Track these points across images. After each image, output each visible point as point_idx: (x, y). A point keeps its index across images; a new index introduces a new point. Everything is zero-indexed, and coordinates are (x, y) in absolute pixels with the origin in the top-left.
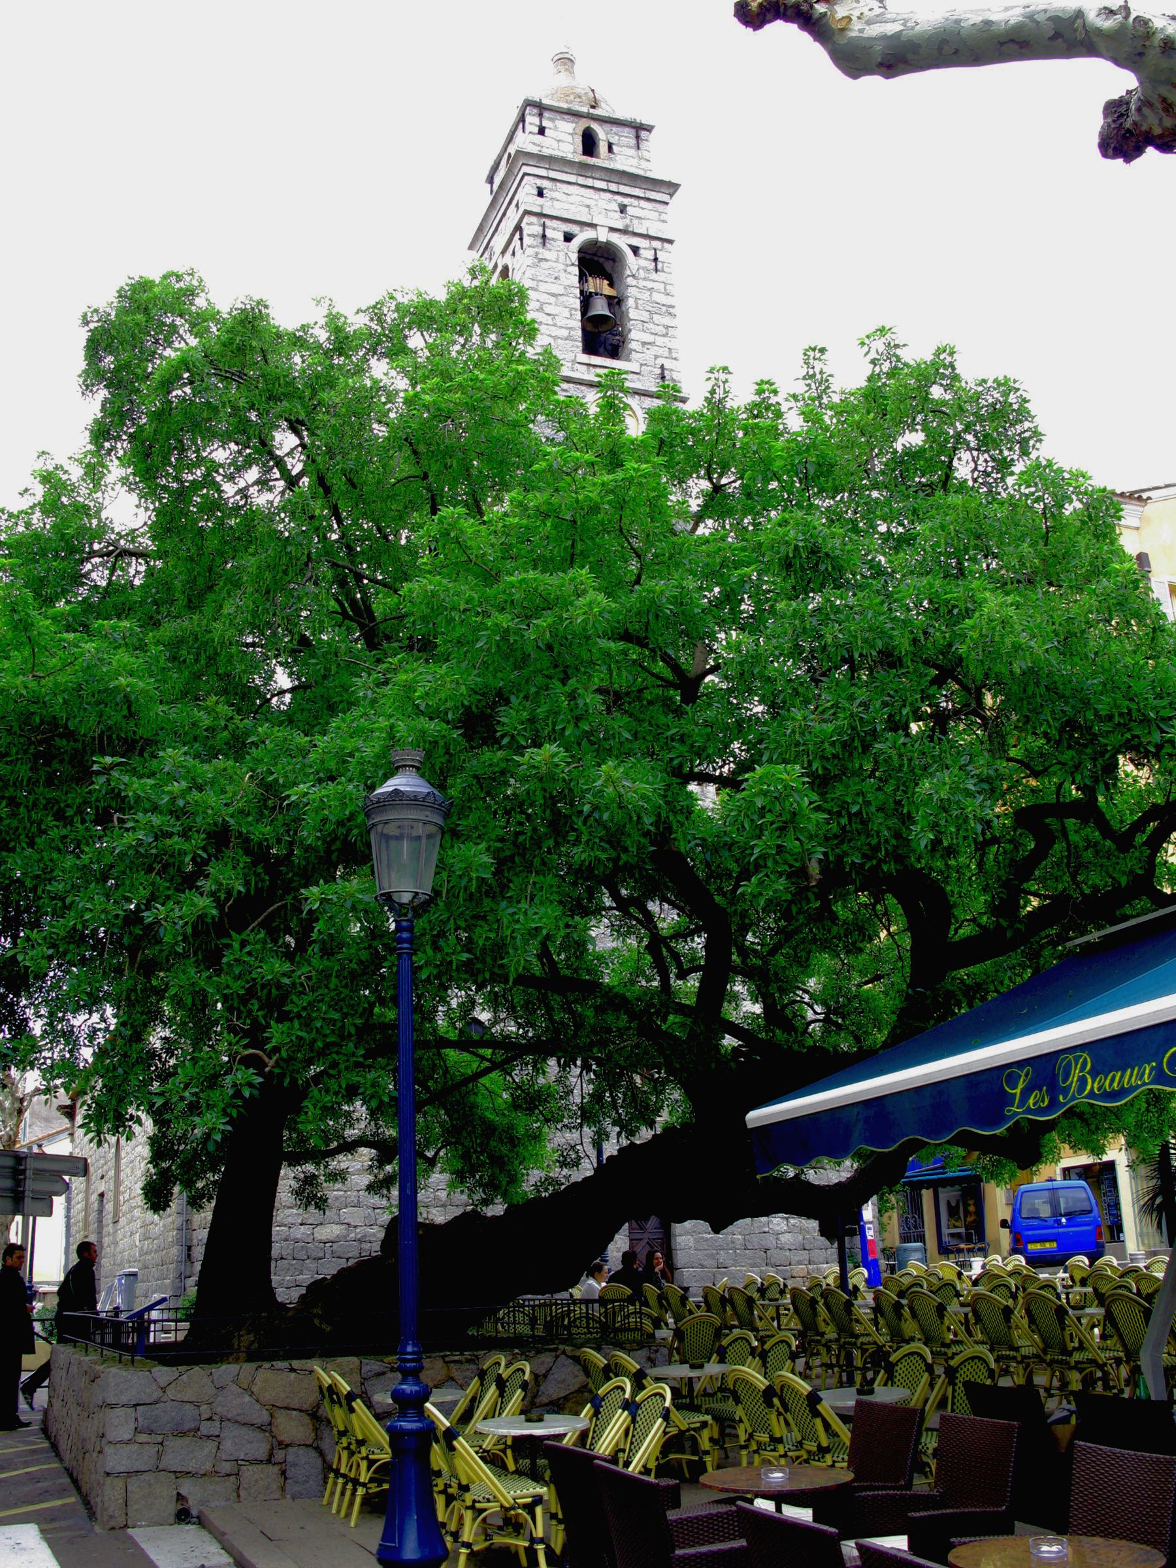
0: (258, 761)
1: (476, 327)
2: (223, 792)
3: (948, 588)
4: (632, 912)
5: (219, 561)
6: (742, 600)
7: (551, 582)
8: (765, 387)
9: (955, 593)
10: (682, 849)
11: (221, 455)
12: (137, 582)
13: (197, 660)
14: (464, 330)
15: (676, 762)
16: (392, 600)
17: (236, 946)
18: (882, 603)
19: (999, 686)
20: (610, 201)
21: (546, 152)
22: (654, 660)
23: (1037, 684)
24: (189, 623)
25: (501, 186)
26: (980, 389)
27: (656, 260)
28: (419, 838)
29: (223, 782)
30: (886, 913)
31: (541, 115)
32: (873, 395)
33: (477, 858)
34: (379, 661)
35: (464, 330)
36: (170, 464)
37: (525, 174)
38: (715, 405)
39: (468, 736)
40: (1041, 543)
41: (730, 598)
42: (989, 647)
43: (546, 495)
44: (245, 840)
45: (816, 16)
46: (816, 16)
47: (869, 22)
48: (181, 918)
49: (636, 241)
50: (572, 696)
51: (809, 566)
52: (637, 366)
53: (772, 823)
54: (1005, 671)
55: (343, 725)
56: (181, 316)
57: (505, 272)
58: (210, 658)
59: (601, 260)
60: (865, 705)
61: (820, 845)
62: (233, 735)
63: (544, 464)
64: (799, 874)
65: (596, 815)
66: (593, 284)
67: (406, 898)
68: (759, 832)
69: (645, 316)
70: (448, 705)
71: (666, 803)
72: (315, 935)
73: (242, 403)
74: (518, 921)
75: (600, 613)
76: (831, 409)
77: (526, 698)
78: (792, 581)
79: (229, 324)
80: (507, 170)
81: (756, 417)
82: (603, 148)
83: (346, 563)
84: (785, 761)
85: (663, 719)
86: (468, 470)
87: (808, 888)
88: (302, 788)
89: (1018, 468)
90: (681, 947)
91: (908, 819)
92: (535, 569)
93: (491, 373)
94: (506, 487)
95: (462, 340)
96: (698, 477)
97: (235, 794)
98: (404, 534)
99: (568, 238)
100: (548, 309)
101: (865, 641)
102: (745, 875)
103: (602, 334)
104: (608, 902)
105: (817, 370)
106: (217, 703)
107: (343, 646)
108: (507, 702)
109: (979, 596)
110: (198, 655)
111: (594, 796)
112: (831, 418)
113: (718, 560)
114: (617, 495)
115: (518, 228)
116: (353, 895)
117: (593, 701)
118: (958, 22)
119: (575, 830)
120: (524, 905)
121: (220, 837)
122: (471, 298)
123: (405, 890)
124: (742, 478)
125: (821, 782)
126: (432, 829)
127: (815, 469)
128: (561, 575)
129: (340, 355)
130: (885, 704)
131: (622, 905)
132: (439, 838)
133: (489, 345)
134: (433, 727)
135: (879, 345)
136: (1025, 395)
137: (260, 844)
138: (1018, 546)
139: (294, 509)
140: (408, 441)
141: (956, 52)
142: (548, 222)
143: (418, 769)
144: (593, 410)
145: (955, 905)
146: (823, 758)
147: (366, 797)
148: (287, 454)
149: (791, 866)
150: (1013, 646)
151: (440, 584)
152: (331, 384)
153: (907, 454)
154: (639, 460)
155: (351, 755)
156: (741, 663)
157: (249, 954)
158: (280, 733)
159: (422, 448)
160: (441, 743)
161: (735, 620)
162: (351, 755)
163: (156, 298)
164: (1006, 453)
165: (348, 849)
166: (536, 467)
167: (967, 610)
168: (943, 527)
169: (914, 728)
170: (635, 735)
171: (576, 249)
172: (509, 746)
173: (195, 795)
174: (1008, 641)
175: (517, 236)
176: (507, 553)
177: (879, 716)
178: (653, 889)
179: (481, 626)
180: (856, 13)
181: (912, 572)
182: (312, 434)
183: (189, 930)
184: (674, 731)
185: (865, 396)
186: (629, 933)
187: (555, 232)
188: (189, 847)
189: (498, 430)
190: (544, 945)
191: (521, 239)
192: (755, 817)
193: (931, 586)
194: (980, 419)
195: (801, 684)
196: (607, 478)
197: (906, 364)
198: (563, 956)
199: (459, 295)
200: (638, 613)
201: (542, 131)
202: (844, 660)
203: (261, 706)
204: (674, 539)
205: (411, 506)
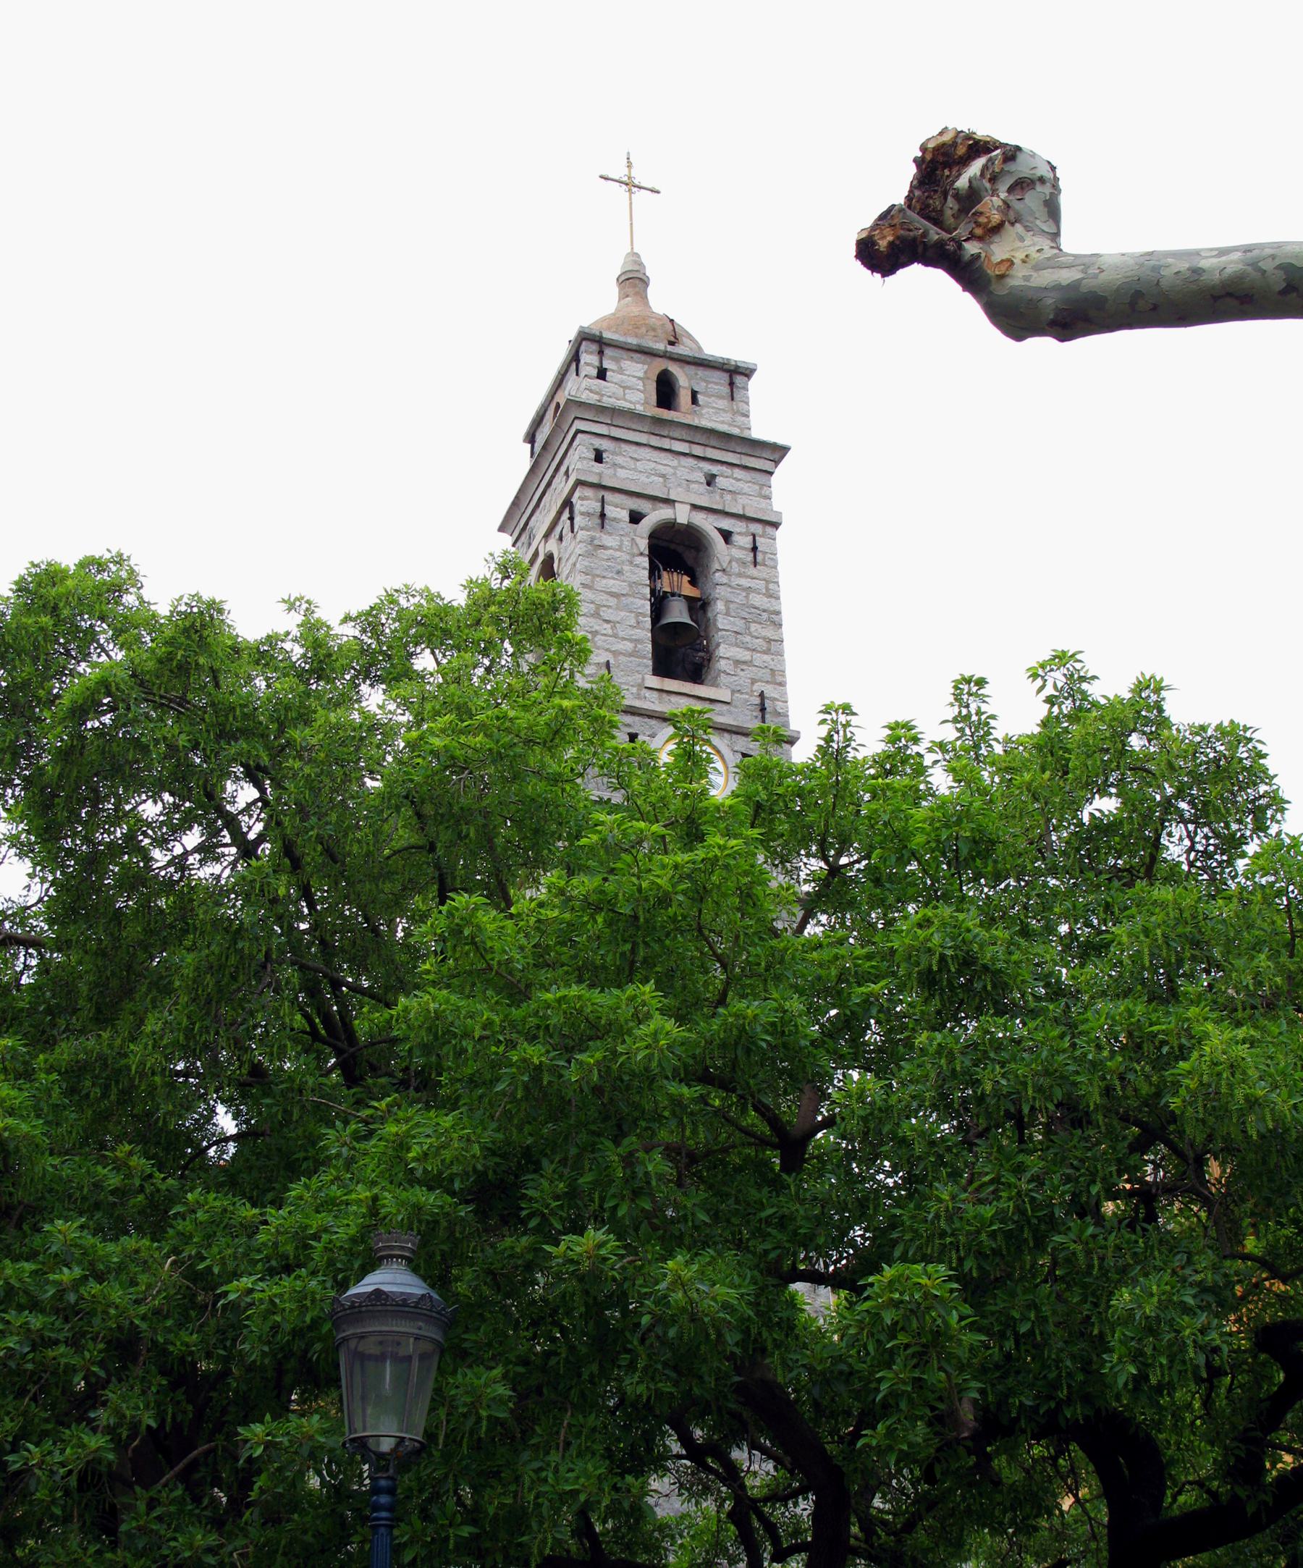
0: (186, 1238)
1: (507, 644)
2: (133, 1283)
3: (1154, 1017)
4: (709, 1463)
5: (142, 956)
6: (868, 1027)
7: (601, 1000)
8: (902, 733)
9: (1165, 1023)
10: (780, 1379)
11: (150, 810)
12: (25, 980)
13: (105, 1095)
14: (489, 648)
15: (772, 1255)
16: (380, 1016)
17: (142, 1507)
18: (1062, 1036)
19: (1228, 1151)
20: (692, 469)
21: (608, 402)
22: (744, 1111)
23: (1282, 1153)
24: (94, 1044)
25: (544, 448)
26: (1198, 739)
27: (754, 549)
28: (409, 1359)
29: (134, 1268)
30: (1073, 1471)
31: (601, 353)
32: (1050, 745)
33: (491, 1385)
34: (359, 1103)
35: (489, 648)
36: (80, 821)
37: (578, 432)
38: (833, 754)
39: (482, 1214)
40: (1285, 953)
41: (851, 1024)
42: (1211, 1096)
43: (597, 881)
44: (161, 1351)
45: (967, 257)
46: (967, 257)
47: (1038, 268)
48: (63, 1465)
49: (726, 524)
50: (629, 1161)
51: (960, 983)
52: (727, 689)
53: (907, 1346)
54: (1236, 1134)
55: (307, 1195)
56: (102, 619)
57: (548, 570)
58: (122, 1092)
59: (680, 549)
60: (1038, 1180)
61: (975, 1378)
62: (150, 1199)
63: (595, 838)
64: (941, 1420)
65: (659, 1330)
66: (667, 581)
67: (386, 1445)
68: (887, 1359)
69: (739, 625)
70: (455, 1169)
71: (758, 1314)
72: (253, 1495)
73: (183, 741)
74: (545, 1480)
75: (669, 1047)
76: (993, 764)
77: (563, 1162)
78: (936, 1003)
79: (168, 633)
80: (552, 428)
81: (888, 773)
82: (684, 398)
83: (320, 964)
84: (927, 1259)
85: (754, 1194)
86: (490, 841)
87: (958, 1441)
88: (246, 1282)
89: (1252, 848)
90: (779, 1513)
91: (1101, 1344)
92: (580, 981)
93: (525, 708)
94: (541, 863)
95: (487, 662)
96: (808, 855)
97: (149, 1286)
98: (401, 925)
99: (635, 518)
100: (606, 614)
101: (1039, 1089)
102: (867, 1419)
103: (681, 650)
104: (676, 1448)
105: (973, 709)
106: (130, 1153)
107: (311, 1081)
108: (538, 1169)
109: (1197, 1029)
110: (106, 1088)
111: (657, 1303)
112: (992, 775)
113: (834, 972)
114: (694, 882)
115: (568, 503)
116: (311, 1438)
117: (656, 1164)
118: (1156, 269)
119: (628, 1351)
120: (554, 1457)
121: (125, 1348)
122: (500, 604)
123: (386, 1433)
124: (868, 857)
125: (974, 1290)
126: (428, 1347)
127: (969, 847)
128: (616, 992)
129: (319, 678)
130: (1068, 1179)
131: (695, 1452)
132: (436, 1358)
133: (525, 668)
134: (430, 1200)
135: (1058, 677)
136: (1260, 747)
137: (182, 1360)
138: (1252, 958)
139: (250, 890)
140: (411, 799)
141: (1155, 308)
142: (609, 497)
143: (409, 1260)
144: (664, 758)
145: (1172, 1462)
146: (980, 1254)
147: (335, 1300)
148: (241, 812)
149: (933, 1409)
150: (1247, 1098)
151: (447, 1001)
152: (305, 718)
153: (1096, 827)
154: (728, 834)
155: (316, 1237)
156: (864, 1119)
157: (159, 1519)
158: (216, 1201)
159: (428, 809)
160: (444, 1224)
161: (858, 1056)
162: (316, 1237)
163: (69, 593)
164: (1234, 827)
165: (307, 1365)
166: (584, 841)
167: (1181, 1047)
168: (1146, 931)
169: (1109, 1207)
170: (716, 1216)
171: (646, 535)
172: (537, 1230)
173: (94, 1288)
174: (1239, 1094)
175: (566, 514)
176: (541, 958)
177: (1058, 1193)
178: (738, 1432)
179: (503, 1061)
180: (1020, 255)
181: (1104, 994)
182: (277, 785)
183: (73, 1481)
184: (770, 1211)
185: (1039, 748)
186: (706, 1490)
187: (618, 511)
188: (78, 1363)
189: (535, 787)
190: (583, 1514)
191: (571, 519)
192: (883, 1337)
193: (1131, 1014)
194: (1198, 779)
195: (949, 1149)
196: (681, 858)
197: (1095, 704)
198: (609, 1525)
199: (483, 599)
200: (723, 1045)
201: (602, 374)
202: (1008, 1116)
203: (192, 1158)
204: (774, 942)
205: (411, 887)
